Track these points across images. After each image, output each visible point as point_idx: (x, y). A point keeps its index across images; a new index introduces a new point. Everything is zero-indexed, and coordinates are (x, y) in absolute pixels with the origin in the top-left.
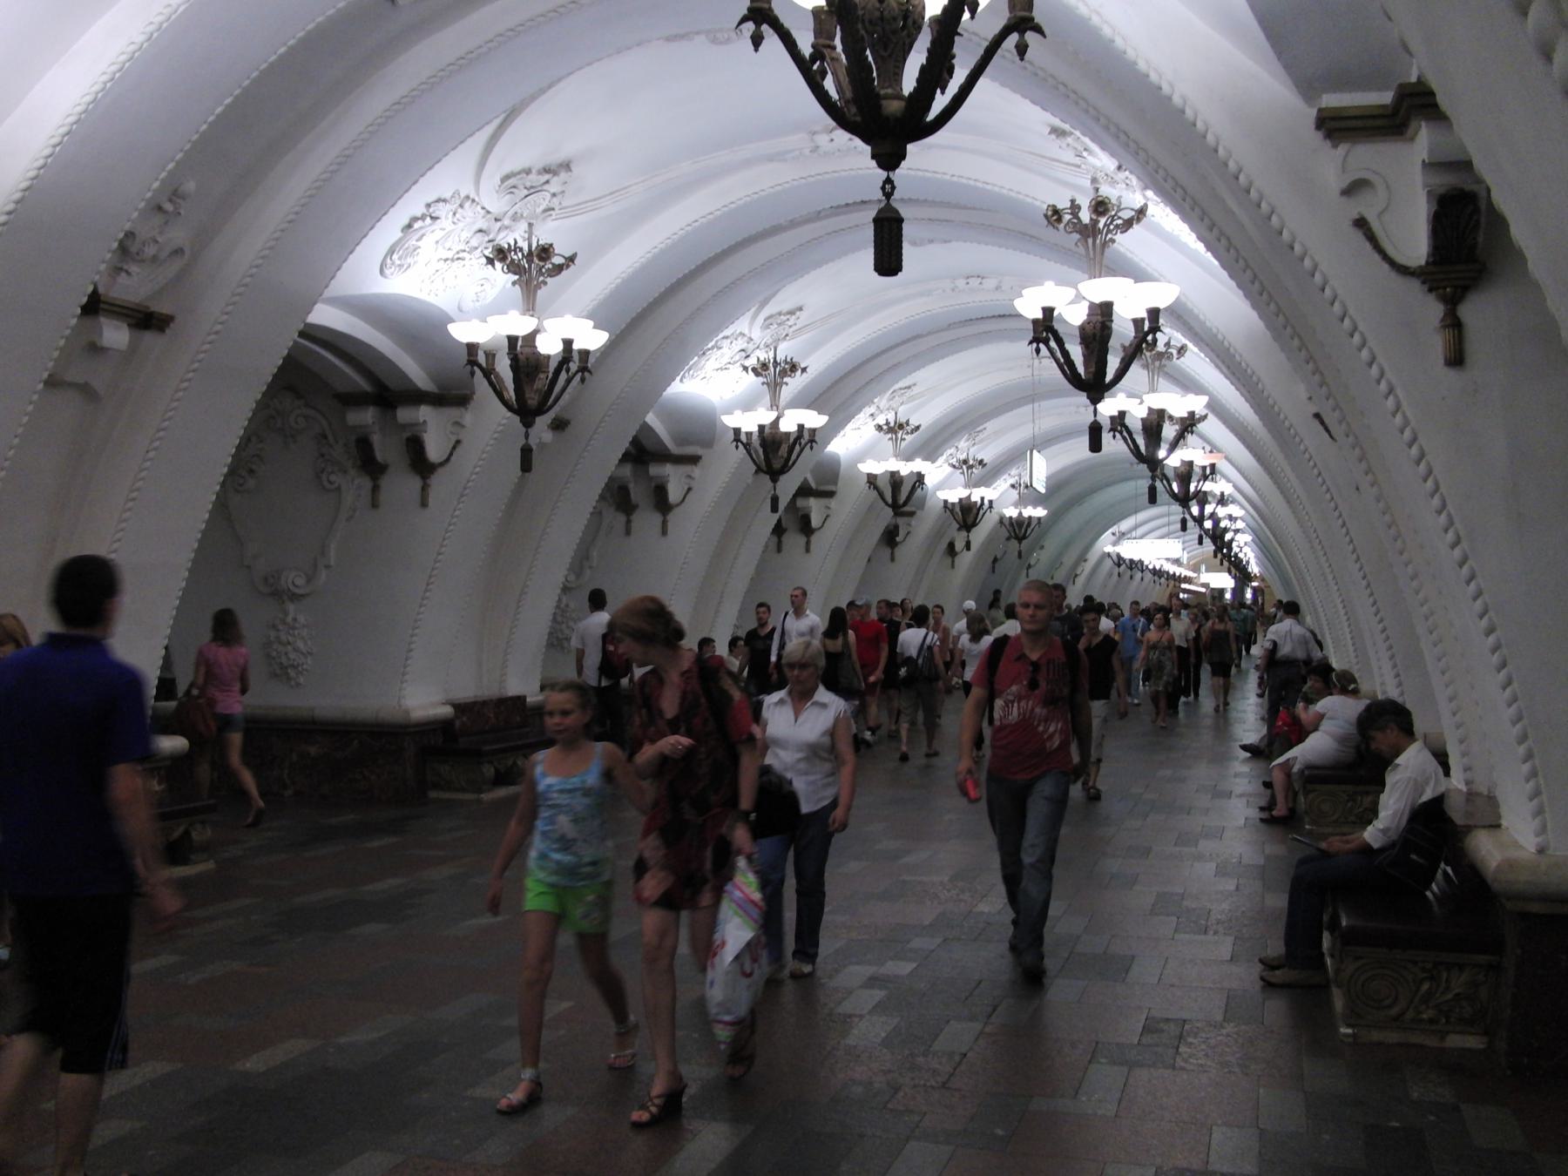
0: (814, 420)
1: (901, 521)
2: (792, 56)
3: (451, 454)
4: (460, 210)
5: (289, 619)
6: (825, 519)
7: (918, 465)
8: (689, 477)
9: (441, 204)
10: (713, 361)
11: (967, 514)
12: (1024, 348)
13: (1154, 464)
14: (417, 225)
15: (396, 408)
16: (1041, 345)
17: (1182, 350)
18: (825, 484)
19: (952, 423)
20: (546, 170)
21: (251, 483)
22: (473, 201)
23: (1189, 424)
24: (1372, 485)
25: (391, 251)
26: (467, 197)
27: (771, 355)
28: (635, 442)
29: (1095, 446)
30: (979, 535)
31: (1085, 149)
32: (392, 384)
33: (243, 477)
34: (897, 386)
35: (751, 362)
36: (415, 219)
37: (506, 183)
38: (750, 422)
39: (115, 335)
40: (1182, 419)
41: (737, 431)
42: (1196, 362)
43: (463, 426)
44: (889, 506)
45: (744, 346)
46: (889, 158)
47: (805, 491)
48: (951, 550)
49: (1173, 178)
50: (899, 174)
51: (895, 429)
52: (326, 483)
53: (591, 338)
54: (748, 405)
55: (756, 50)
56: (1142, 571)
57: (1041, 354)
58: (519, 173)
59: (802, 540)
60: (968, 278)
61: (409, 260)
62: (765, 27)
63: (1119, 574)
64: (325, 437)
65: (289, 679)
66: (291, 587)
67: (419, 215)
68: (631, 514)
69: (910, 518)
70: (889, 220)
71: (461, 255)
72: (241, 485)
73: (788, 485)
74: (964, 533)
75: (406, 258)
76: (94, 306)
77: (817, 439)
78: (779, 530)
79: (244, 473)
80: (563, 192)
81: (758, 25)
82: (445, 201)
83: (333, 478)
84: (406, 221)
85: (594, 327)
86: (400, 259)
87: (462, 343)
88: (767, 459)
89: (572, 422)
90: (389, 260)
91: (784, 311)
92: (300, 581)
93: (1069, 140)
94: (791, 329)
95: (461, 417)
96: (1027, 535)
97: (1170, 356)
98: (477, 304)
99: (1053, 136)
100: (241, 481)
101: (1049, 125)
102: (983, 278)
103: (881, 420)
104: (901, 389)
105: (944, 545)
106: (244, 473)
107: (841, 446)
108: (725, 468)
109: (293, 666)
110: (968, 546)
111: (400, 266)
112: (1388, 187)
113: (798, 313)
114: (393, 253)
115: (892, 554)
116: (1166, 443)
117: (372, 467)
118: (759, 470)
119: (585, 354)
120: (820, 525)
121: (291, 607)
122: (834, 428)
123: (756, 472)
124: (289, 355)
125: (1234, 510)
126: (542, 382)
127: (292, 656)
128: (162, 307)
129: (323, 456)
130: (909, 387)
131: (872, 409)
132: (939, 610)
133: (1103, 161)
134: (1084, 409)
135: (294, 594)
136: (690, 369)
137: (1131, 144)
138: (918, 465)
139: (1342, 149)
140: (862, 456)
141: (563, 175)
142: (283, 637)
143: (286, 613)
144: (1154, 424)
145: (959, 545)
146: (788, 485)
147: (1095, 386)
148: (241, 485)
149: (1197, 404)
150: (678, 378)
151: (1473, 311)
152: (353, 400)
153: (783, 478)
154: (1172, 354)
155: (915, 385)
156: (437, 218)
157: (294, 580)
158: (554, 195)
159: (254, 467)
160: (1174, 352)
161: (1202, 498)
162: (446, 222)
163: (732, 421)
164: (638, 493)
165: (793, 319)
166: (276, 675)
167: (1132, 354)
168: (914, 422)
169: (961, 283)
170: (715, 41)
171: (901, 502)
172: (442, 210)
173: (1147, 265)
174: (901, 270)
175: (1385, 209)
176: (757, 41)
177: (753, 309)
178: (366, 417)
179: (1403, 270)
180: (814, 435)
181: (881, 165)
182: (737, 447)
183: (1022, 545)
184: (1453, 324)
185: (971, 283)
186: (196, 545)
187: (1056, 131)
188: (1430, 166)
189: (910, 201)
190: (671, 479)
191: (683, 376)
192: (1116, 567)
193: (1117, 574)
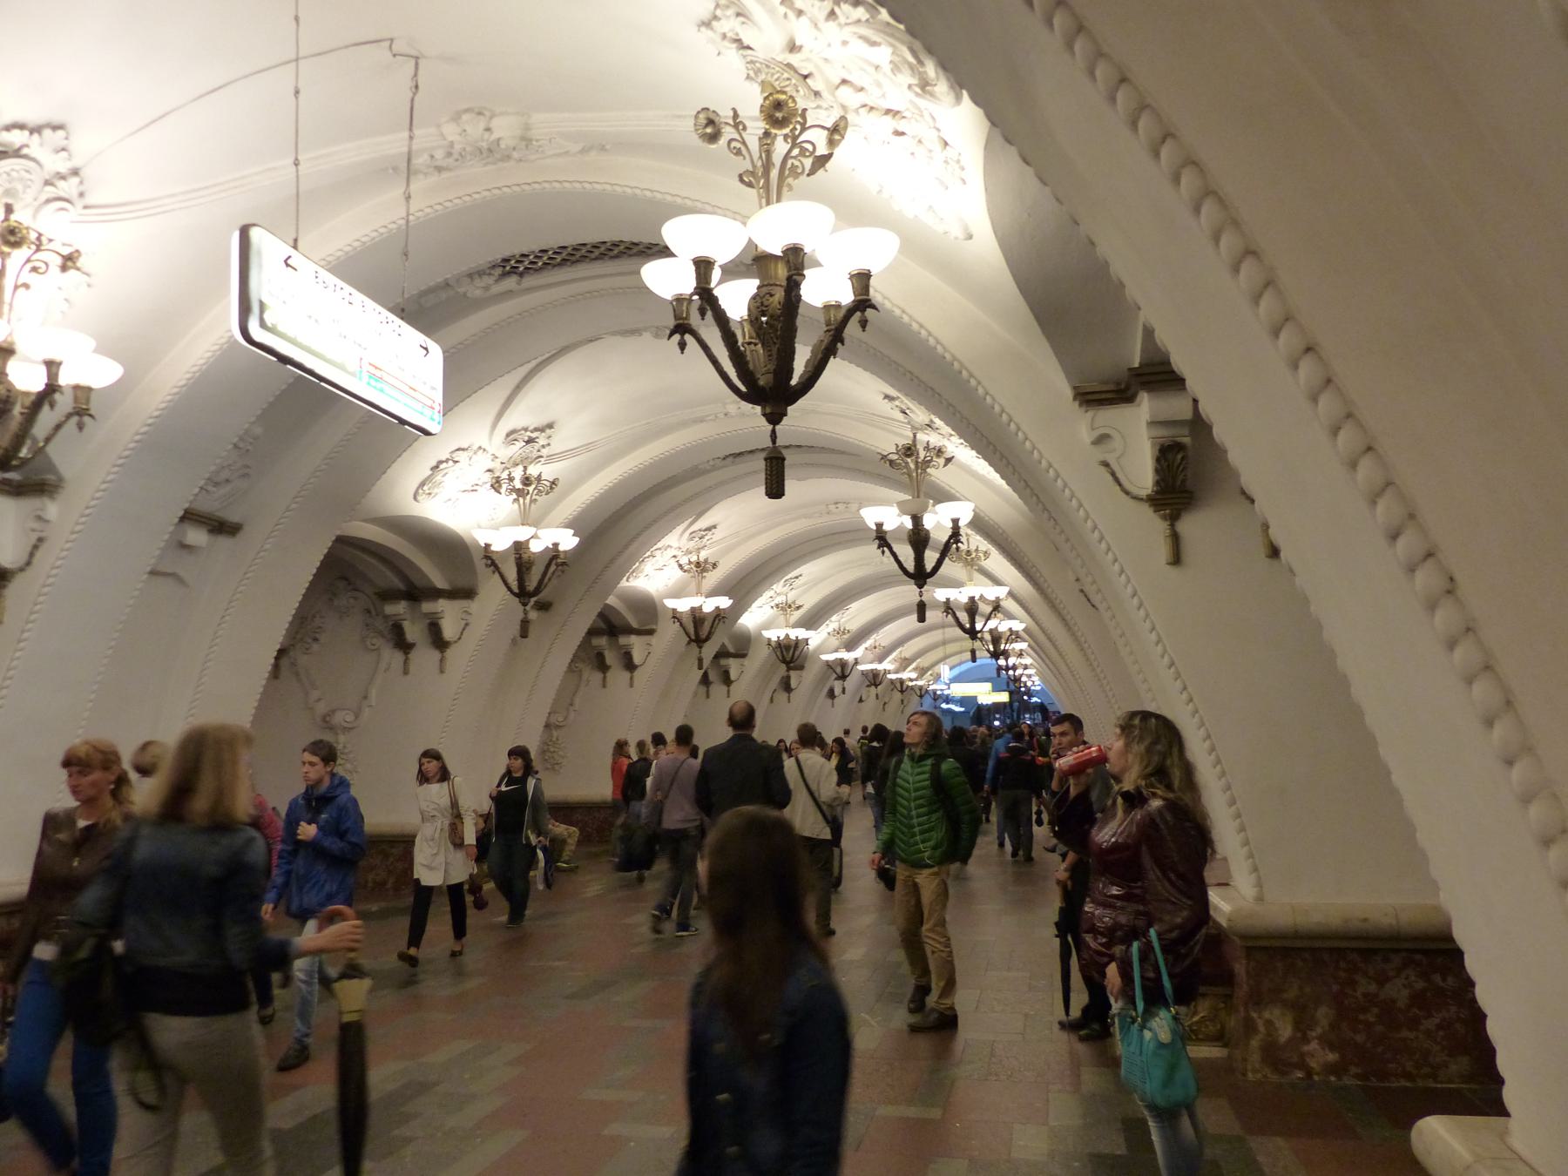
1: (792, 673)
2: (707, 355)
3: (32, 555)
5: (554, 739)
6: (464, 629)
8: (39, 518)
9: (461, 452)
10: (649, 567)
12: (873, 548)
13: (972, 633)
14: (442, 466)
15: (617, 637)
17: (986, 554)
18: (742, 646)
20: (706, 530)
21: (315, 647)
22: (484, 450)
23: (997, 607)
24: (1126, 646)
25: (422, 484)
26: (480, 448)
28: (601, 615)
30: (851, 683)
31: (908, 409)
32: (616, 621)
33: (309, 643)
35: (773, 604)
36: (441, 462)
37: (510, 438)
40: (993, 601)
41: (674, 610)
42: (997, 562)
43: (651, 645)
45: (491, 465)
46: (774, 418)
47: (722, 654)
49: (973, 425)
50: (782, 428)
51: (785, 608)
53: (568, 541)
54: (677, 593)
56: (921, 696)
57: (885, 554)
60: (836, 503)
61: (436, 490)
62: (688, 337)
63: (877, 695)
66: (346, 725)
67: (444, 459)
69: (742, 660)
70: (777, 458)
71: (475, 488)
72: (307, 649)
73: (709, 650)
74: (841, 682)
75: (433, 489)
76: (189, 517)
77: (875, 295)
78: (705, 680)
80: (549, 445)
81: (682, 335)
82: (463, 450)
83: (374, 641)
84: (434, 464)
85: (97, 351)
86: (429, 489)
88: (783, 656)
91: (704, 528)
92: (350, 718)
93: (897, 403)
94: (709, 542)
95: (469, 607)
96: (795, 658)
97: (979, 558)
98: (493, 522)
99: (886, 401)
100: (307, 646)
101: (884, 394)
102: (848, 503)
103: (779, 600)
104: (791, 579)
105: (826, 690)
106: (310, 641)
107: (750, 620)
109: (557, 764)
110: (844, 691)
111: (430, 494)
112: (1123, 437)
113: (548, 431)
114: (424, 485)
116: (934, 549)
117: (603, 667)
118: (691, 640)
119: (82, 392)
120: (24, 558)
121: (555, 734)
122: (739, 608)
123: (689, 643)
124: (328, 553)
126: (707, 626)
128: (232, 516)
133: (920, 415)
134: (834, 506)
135: (345, 728)
136: (633, 572)
137: (944, 401)
138: (801, 633)
139: (1090, 414)
141: (548, 431)
144: (972, 608)
145: (837, 691)
146: (709, 650)
147: (920, 576)
148: (307, 649)
149: (1001, 592)
150: (625, 578)
152: (388, 596)
154: (980, 557)
155: (801, 575)
158: (543, 446)
159: (317, 635)
161: (1006, 654)
163: (670, 603)
164: (712, 676)
165: (797, 580)
166: (547, 769)
168: (799, 603)
169: (832, 507)
171: (704, 637)
172: (460, 456)
174: (784, 495)
175: (1122, 455)
176: (682, 346)
177: (690, 520)
178: (399, 608)
179: (1136, 498)
182: (682, 346)
183: (704, 650)
184: (1175, 539)
186: (261, 690)
187: (887, 397)
188: (1153, 424)
189: (786, 447)
190: (732, 666)
193: (875, 696)
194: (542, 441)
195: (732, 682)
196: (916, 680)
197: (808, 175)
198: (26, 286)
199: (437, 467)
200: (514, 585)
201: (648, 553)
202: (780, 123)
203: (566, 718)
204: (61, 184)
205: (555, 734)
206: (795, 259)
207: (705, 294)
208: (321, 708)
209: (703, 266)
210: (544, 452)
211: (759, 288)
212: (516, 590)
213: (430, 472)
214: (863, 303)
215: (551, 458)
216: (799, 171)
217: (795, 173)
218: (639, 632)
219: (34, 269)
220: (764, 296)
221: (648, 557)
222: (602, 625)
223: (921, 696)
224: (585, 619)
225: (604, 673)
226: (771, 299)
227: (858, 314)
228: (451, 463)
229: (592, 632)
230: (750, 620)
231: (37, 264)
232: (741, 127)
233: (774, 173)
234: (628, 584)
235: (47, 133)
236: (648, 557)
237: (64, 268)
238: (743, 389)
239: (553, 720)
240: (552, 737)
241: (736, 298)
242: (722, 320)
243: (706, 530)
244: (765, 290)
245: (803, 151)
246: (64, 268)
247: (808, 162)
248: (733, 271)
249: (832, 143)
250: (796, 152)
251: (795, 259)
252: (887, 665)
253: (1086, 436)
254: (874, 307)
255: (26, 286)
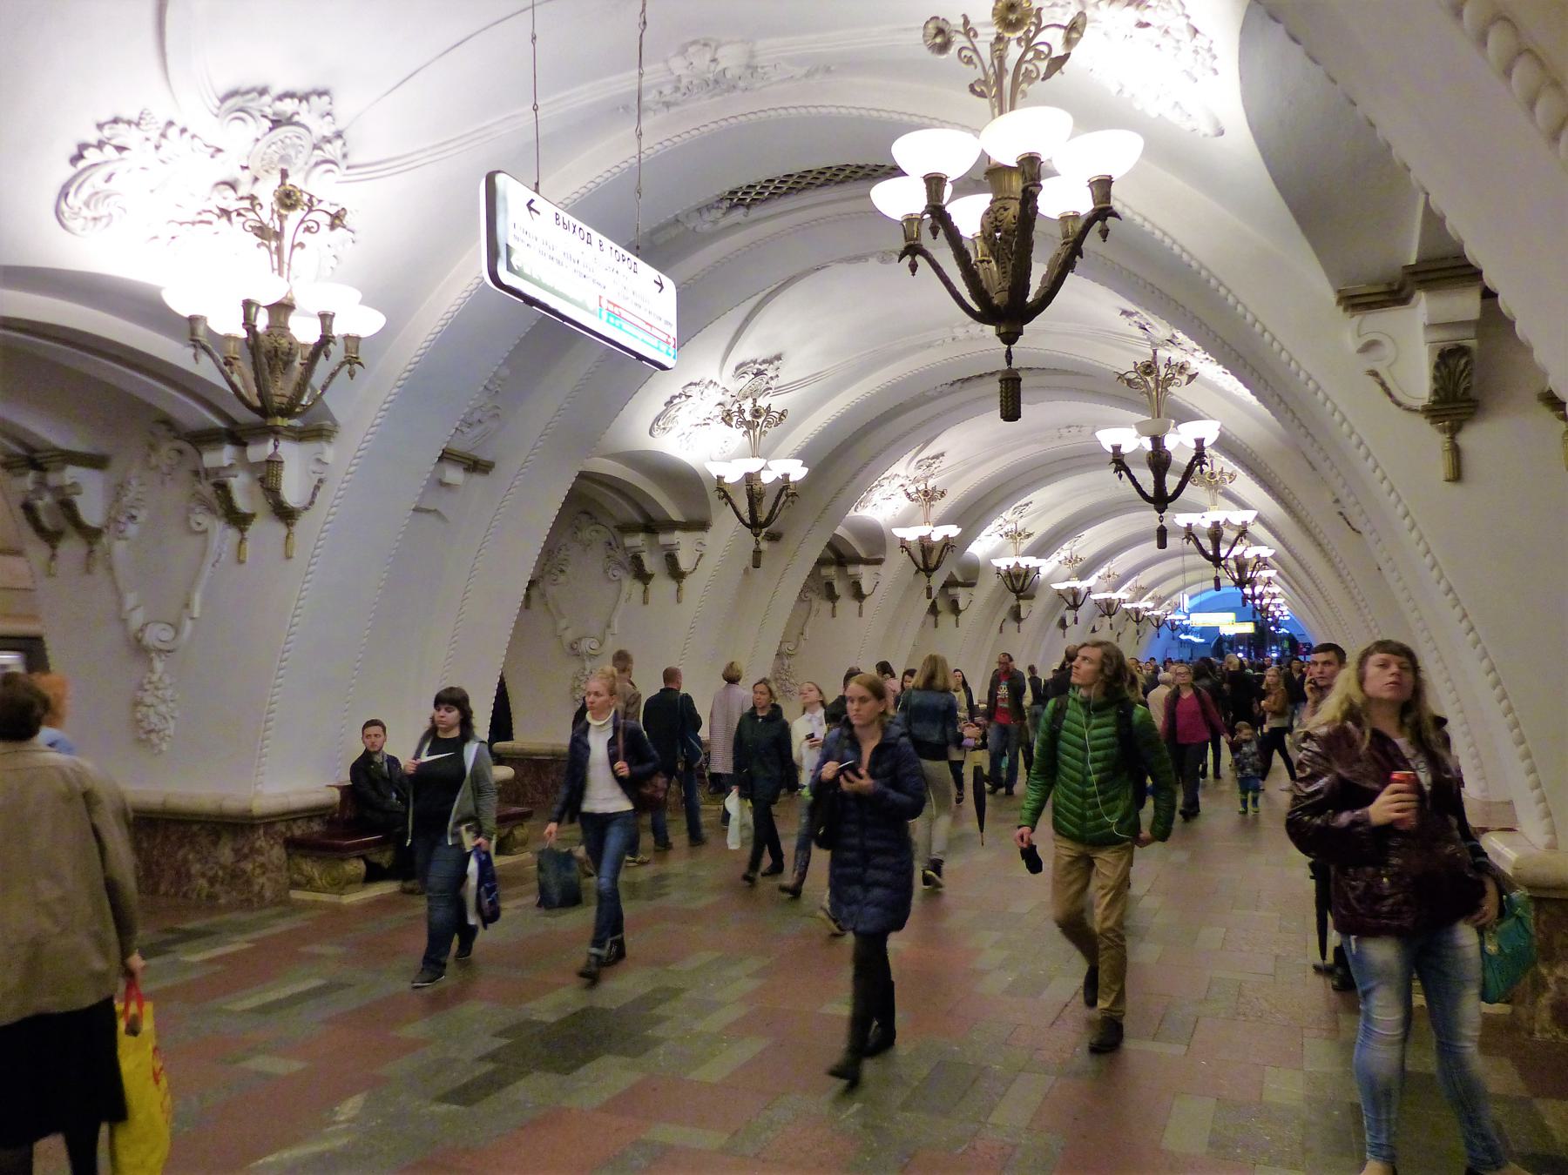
0: (953, 531)
3: (314, 495)
4: (164, 141)
7: (1032, 562)
9: (693, 387)
10: (877, 496)
11: (1074, 600)
13: (1216, 560)
14: (675, 402)
16: (1123, 472)
17: (1232, 476)
18: (971, 576)
19: (1063, 529)
20: (933, 458)
22: (715, 384)
23: (1243, 533)
25: (658, 419)
26: (711, 382)
27: (1014, 526)
28: (830, 545)
29: (1218, 587)
30: (1083, 612)
34: (1016, 505)
36: (674, 397)
38: (1003, 563)
39: (454, 475)
41: (903, 540)
42: (1244, 485)
44: (747, 525)
45: (721, 398)
46: (1010, 338)
47: (951, 583)
48: (1063, 624)
51: (1015, 536)
52: (611, 577)
53: (797, 471)
54: (905, 523)
55: (913, 275)
56: (1158, 627)
58: (247, 92)
59: (953, 618)
61: (670, 425)
64: (610, 544)
65: (153, 746)
66: (591, 652)
68: (245, 530)
71: (708, 421)
73: (938, 580)
76: (447, 456)
78: (933, 610)
79: (123, 519)
80: (777, 376)
81: (913, 256)
82: (695, 384)
83: (807, 595)
84: (668, 399)
85: (362, 302)
87: (182, 317)
89: (496, 465)
90: (63, 206)
99: (1124, 316)
103: (1009, 527)
105: (1057, 619)
108: (987, 587)
111: (664, 429)
114: (67, 195)
115: (957, 620)
116: (1176, 473)
117: (832, 596)
119: (352, 341)
123: (917, 572)
125: (1276, 589)
127: (154, 719)
128: (485, 456)
129: (609, 557)
130: (1027, 505)
131: (1000, 521)
132: (1330, 656)
134: (1067, 430)
138: (1032, 562)
139: (1357, 318)
140: (997, 554)
142: (148, 700)
143: (152, 671)
144: (1216, 534)
146: (938, 580)
147: (1161, 500)
149: (1249, 516)
150: (853, 508)
151: (1473, 438)
153: (935, 574)
156: (690, 396)
157: (156, 635)
159: (134, 512)
160: (1227, 477)
162: (695, 399)
164: (941, 605)
167: (1187, 475)
168: (1029, 530)
169: (1064, 431)
170: (883, 261)
171: (763, 519)
172: (693, 391)
173: (1124, 205)
176: (914, 267)
178: (637, 541)
179: (1410, 409)
180: (1107, 196)
181: (1004, 341)
184: (1456, 452)
185: (971, 331)
190: (682, 546)
191: (857, 507)
192: (922, 574)
194: (770, 373)
195: (960, 612)
196: (1153, 609)
197: (1043, 79)
198: (302, 245)
199: (671, 402)
200: (746, 516)
201: (876, 483)
202: (1011, 26)
203: (797, 647)
204: (327, 147)
205: (588, 665)
206: (1031, 169)
207: (938, 214)
208: (569, 636)
209: (934, 183)
210: (773, 384)
211: (992, 202)
212: (748, 522)
213: (70, 171)
214: (1104, 212)
215: (779, 390)
216: (1034, 75)
217: (1029, 79)
218: (867, 562)
219: (308, 229)
220: (1254, 617)
221: (876, 486)
222: (831, 555)
223: (1158, 627)
224: (815, 550)
225: (834, 603)
226: (1006, 213)
227: (1098, 224)
228: (109, 150)
229: (821, 562)
230: (982, 547)
231: (311, 224)
232: (972, 34)
233: (1007, 81)
234: (856, 514)
235: (314, 99)
236: (876, 486)
237: (332, 227)
238: (977, 309)
239: (785, 647)
240: (585, 669)
241: (969, 215)
242: (954, 237)
243: (933, 458)
244: (998, 204)
245: (1038, 54)
246: (332, 227)
247: (1043, 66)
248: (966, 186)
249: (1069, 42)
250: (1030, 55)
251: (1031, 169)
252: (1122, 594)
253: (1351, 342)
254: (1115, 215)
255: (302, 245)
